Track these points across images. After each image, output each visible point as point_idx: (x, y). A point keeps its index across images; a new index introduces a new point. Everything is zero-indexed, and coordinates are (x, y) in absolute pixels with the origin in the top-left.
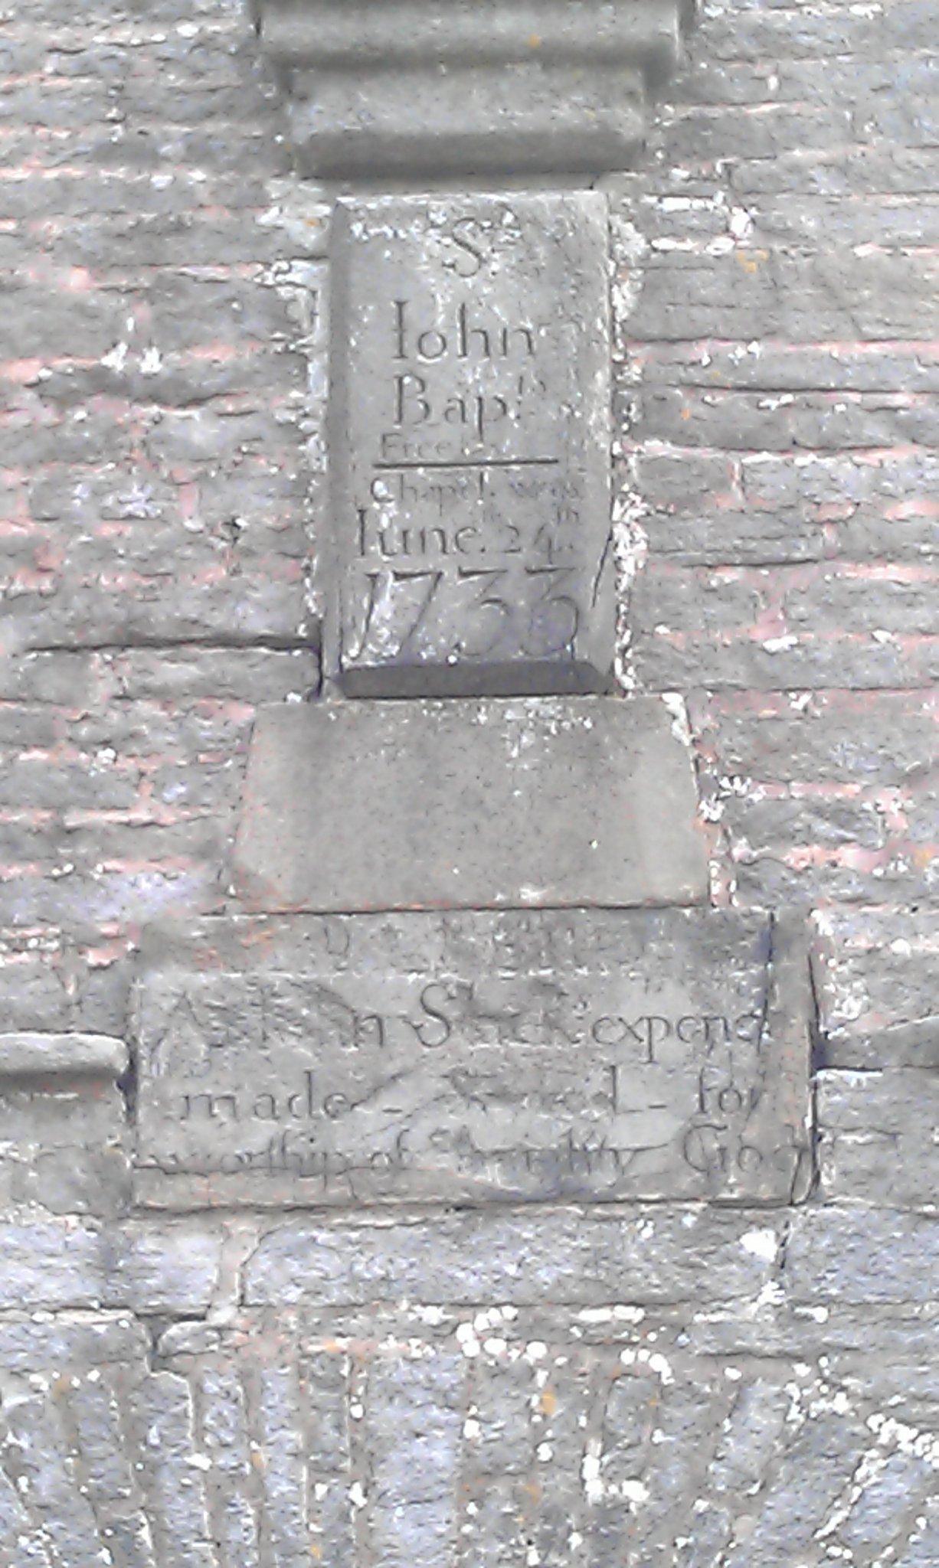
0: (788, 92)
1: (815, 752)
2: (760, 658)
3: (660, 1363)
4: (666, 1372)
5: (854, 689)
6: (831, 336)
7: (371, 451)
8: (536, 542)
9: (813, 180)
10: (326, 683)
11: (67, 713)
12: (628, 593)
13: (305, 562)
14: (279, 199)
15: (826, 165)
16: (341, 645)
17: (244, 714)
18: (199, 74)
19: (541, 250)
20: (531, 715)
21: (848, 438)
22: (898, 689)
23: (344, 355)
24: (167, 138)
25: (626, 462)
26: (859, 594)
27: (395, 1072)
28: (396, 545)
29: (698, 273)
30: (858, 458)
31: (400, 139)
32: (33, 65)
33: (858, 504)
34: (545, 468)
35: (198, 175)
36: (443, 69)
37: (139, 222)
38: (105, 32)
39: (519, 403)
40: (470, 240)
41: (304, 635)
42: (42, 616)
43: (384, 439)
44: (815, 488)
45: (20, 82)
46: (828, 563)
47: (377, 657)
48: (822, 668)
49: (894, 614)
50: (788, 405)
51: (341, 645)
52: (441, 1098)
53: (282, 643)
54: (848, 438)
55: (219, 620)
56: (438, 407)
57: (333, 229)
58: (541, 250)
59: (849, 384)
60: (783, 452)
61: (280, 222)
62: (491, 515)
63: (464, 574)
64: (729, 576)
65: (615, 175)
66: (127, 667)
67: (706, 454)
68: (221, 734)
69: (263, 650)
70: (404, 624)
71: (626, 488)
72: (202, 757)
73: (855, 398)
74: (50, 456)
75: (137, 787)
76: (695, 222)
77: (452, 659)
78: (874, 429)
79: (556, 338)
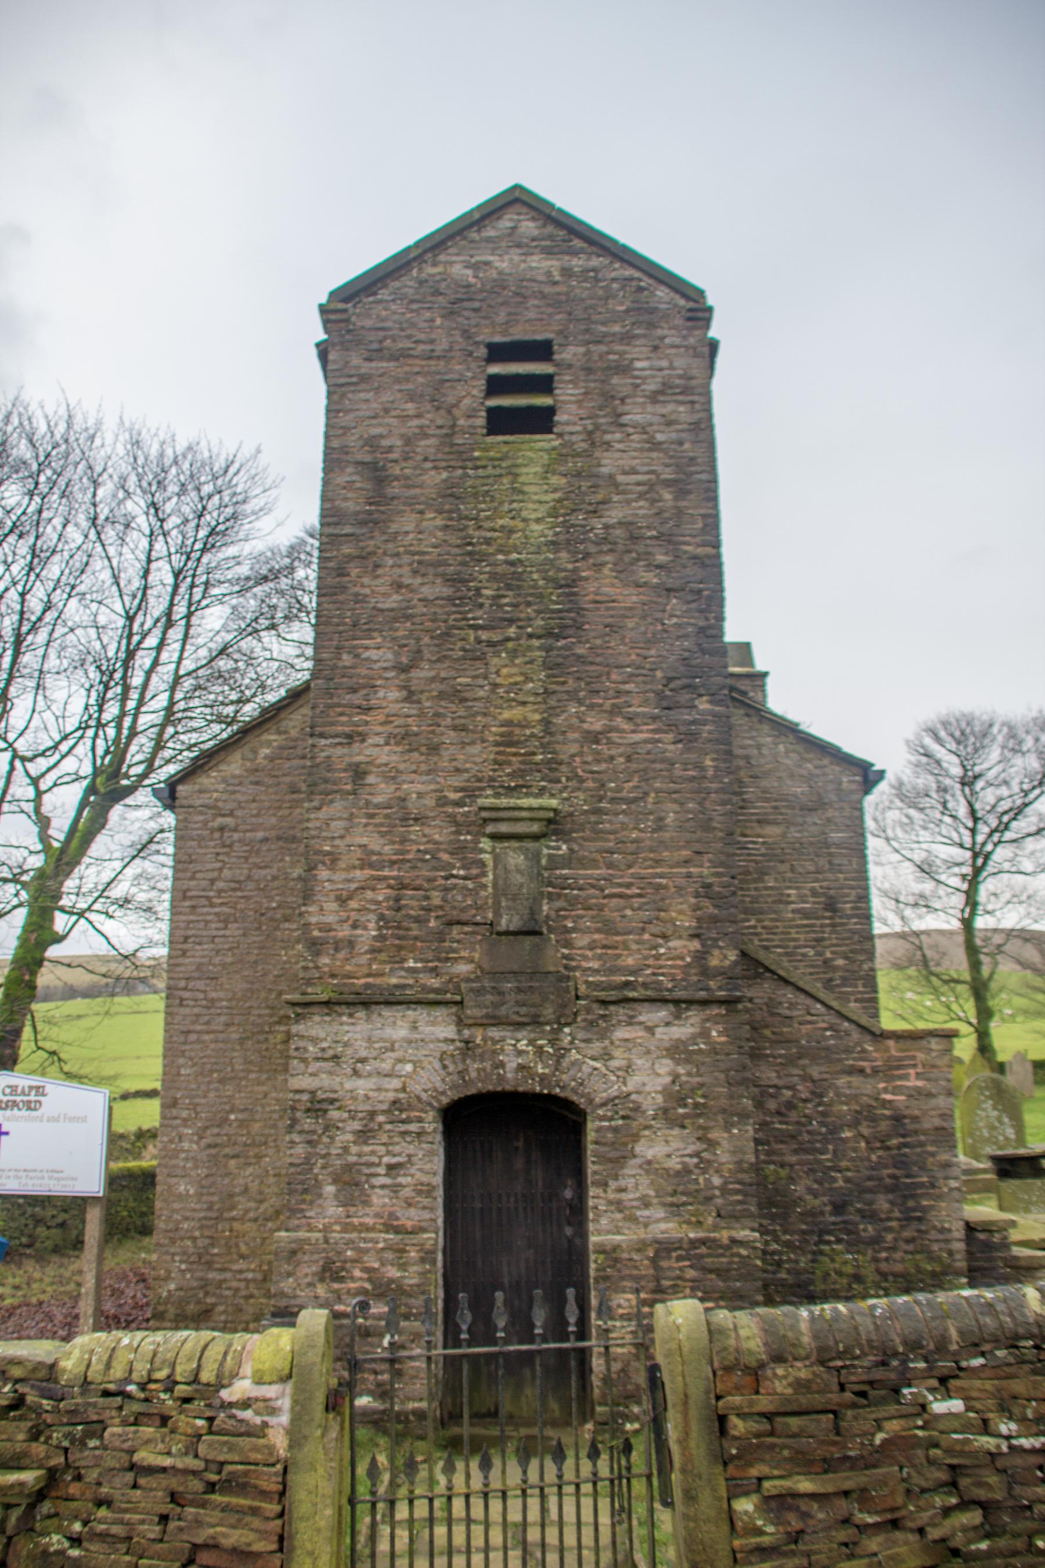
27: (223, 465)
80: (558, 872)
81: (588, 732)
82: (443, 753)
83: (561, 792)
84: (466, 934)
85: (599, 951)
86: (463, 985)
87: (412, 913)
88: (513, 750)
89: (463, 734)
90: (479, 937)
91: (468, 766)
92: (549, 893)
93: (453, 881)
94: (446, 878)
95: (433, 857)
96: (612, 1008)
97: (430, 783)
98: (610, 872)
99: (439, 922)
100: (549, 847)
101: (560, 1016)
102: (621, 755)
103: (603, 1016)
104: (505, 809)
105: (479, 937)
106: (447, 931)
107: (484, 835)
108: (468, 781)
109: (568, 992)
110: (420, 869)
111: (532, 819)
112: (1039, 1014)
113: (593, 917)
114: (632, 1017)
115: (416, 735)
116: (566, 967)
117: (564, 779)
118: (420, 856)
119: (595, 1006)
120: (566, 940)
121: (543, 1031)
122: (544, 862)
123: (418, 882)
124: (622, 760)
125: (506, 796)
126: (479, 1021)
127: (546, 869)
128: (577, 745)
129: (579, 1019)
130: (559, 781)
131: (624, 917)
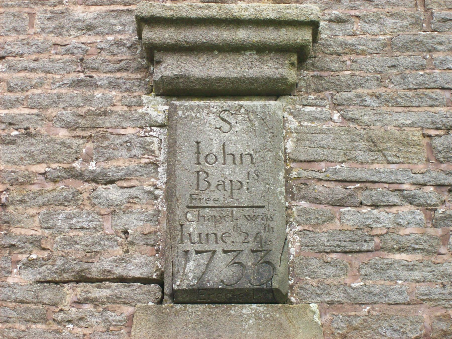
1: (373, 330)
2: (349, 290)
5: (390, 304)
6: (374, 161)
7: (184, 202)
8: (255, 238)
9: (366, 101)
10: (166, 297)
11: (53, 308)
13: (156, 248)
14: (147, 103)
15: (371, 95)
16: (173, 280)
17: (128, 310)
18: (114, 55)
19: (256, 123)
20: (253, 311)
21: (384, 202)
22: (409, 304)
23: (174, 163)
25: (292, 209)
26: (390, 265)
28: (196, 239)
29: (319, 135)
30: (387, 209)
31: (197, 79)
32: (46, 50)
33: (388, 228)
34: (259, 210)
36: (216, 52)
37: (89, 110)
38: (77, 38)
39: (248, 183)
40: (227, 118)
41: (155, 277)
42: (44, 268)
43: (191, 195)
44: (370, 221)
45: (41, 56)
46: (376, 253)
47: (189, 285)
48: (375, 295)
49: (404, 274)
50: (358, 188)
51: (173, 280)
53: (146, 281)
54: (384, 202)
55: (119, 271)
56: (214, 183)
57: (169, 114)
58: (256, 123)
59: (384, 180)
61: (147, 112)
62: (235, 227)
65: (284, 97)
66: (79, 290)
69: (138, 284)
70: (199, 272)
71: (291, 220)
73: (386, 186)
77: (220, 287)
78: (394, 198)
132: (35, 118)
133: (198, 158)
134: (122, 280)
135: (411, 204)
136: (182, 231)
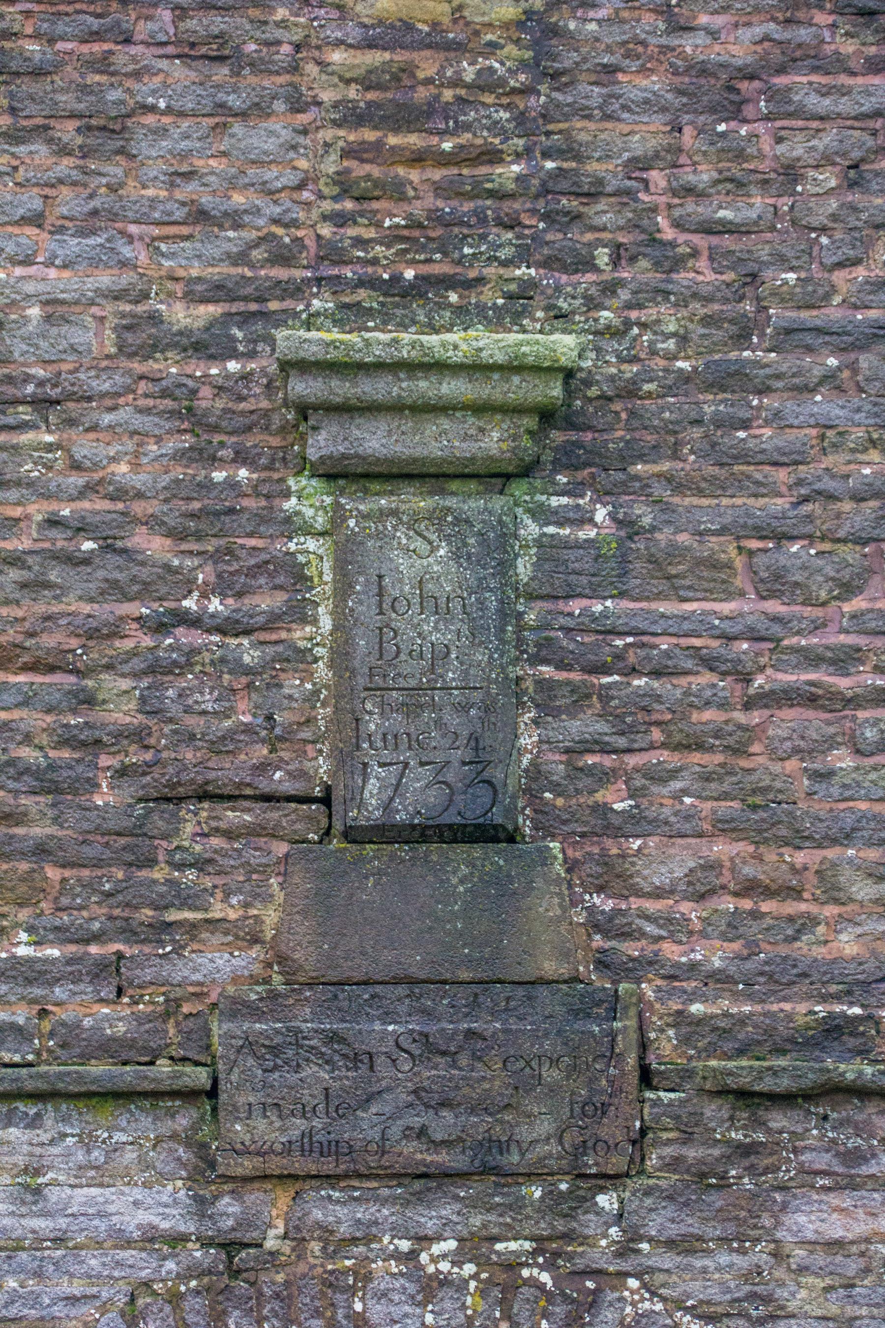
0: (635, 423)
3: (545, 1278)
4: (550, 1284)
6: (659, 596)
12: (526, 771)
24: (222, 444)
35: (243, 473)
42: (148, 778)
47: (368, 819)
50: (630, 644)
52: (410, 1105)
60: (626, 675)
63: (422, 764)
64: (590, 760)
67: (576, 676)
68: (264, 861)
70: (385, 797)
72: (254, 876)
74: (151, 670)
75: (212, 895)
76: (571, 515)
77: (416, 821)
79: (481, 602)
80: (576, 606)
81: (703, 70)
82: (142, 147)
83: (592, 304)
84: (229, 834)
85: (728, 904)
86: (217, 1028)
87: (27, 754)
88: (414, 140)
89: (222, 72)
90: (281, 848)
91: (238, 199)
92: (542, 684)
93: (185, 636)
94: (160, 628)
95: (108, 548)
96: (778, 1120)
97: (95, 263)
98: (773, 606)
99: (128, 792)
100: (541, 514)
101: (582, 1148)
102: (826, 161)
103: (747, 1150)
104: (379, 367)
105: (281, 848)
106: (158, 823)
107: (302, 465)
108: (240, 258)
109: (612, 1056)
110: (60, 591)
111: (481, 409)
112: (10, 380)
113: (707, 778)
114: (854, 1157)
115: (38, 73)
116: (603, 963)
117: (603, 257)
118: (60, 540)
119: (714, 1111)
120: (605, 860)
121: (517, 1205)
122: (524, 569)
123: (49, 641)
124: (829, 179)
125: (385, 319)
126: (275, 1165)
127: (532, 597)
128: (658, 122)
129: (652, 1161)
130: (588, 264)
131: (824, 776)
132: (121, 519)
133: (380, 605)
134: (267, 798)
135: (712, 669)
136: (357, 729)
